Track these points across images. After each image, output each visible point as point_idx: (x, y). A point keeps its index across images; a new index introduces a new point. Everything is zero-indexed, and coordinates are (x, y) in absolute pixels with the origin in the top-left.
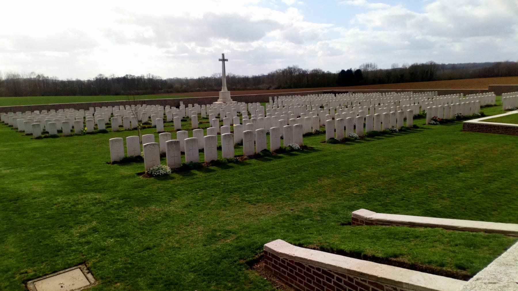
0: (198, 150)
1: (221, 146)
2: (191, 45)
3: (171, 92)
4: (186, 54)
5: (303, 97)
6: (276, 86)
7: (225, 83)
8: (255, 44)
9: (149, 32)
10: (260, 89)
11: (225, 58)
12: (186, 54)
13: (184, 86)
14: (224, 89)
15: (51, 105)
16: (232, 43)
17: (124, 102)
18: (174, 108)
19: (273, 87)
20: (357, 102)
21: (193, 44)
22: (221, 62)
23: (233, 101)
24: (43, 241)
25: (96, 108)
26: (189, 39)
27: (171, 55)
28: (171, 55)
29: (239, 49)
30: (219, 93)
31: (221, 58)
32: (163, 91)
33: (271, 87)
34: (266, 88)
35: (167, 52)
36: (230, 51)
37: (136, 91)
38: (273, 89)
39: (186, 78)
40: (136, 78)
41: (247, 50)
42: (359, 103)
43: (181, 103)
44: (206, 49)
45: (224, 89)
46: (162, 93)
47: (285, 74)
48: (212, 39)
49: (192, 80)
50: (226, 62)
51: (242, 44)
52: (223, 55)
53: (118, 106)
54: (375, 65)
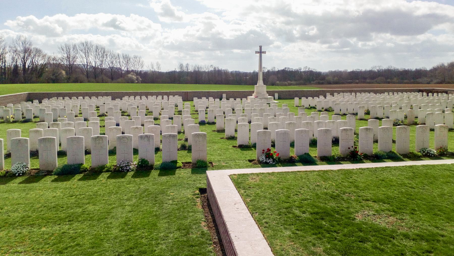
0: (12, 156)
2: (353, 41)
3: (323, 83)
5: (378, 95)
6: (438, 80)
7: (261, 77)
8: (422, 37)
9: (313, 31)
11: (263, 50)
12: (348, 49)
13: (336, 78)
14: (260, 82)
15: (104, 93)
16: (394, 37)
17: (168, 92)
18: (218, 100)
19: (435, 81)
20: (417, 106)
21: (355, 39)
22: (258, 55)
23: (269, 95)
24: (288, 214)
26: (351, 34)
27: (334, 50)
28: (334, 50)
29: (403, 43)
30: (254, 87)
32: (314, 82)
33: (432, 81)
34: (426, 82)
35: (329, 47)
36: (394, 45)
37: (289, 82)
38: (435, 84)
39: (346, 70)
40: (293, 70)
42: (398, 108)
43: (224, 95)
44: (368, 43)
45: (260, 82)
46: (313, 84)
47: (27, 67)
48: (373, 35)
49: (345, 72)
50: (263, 55)
51: (405, 37)
52: (261, 47)
53: (422, 93)
54: (124, 55)
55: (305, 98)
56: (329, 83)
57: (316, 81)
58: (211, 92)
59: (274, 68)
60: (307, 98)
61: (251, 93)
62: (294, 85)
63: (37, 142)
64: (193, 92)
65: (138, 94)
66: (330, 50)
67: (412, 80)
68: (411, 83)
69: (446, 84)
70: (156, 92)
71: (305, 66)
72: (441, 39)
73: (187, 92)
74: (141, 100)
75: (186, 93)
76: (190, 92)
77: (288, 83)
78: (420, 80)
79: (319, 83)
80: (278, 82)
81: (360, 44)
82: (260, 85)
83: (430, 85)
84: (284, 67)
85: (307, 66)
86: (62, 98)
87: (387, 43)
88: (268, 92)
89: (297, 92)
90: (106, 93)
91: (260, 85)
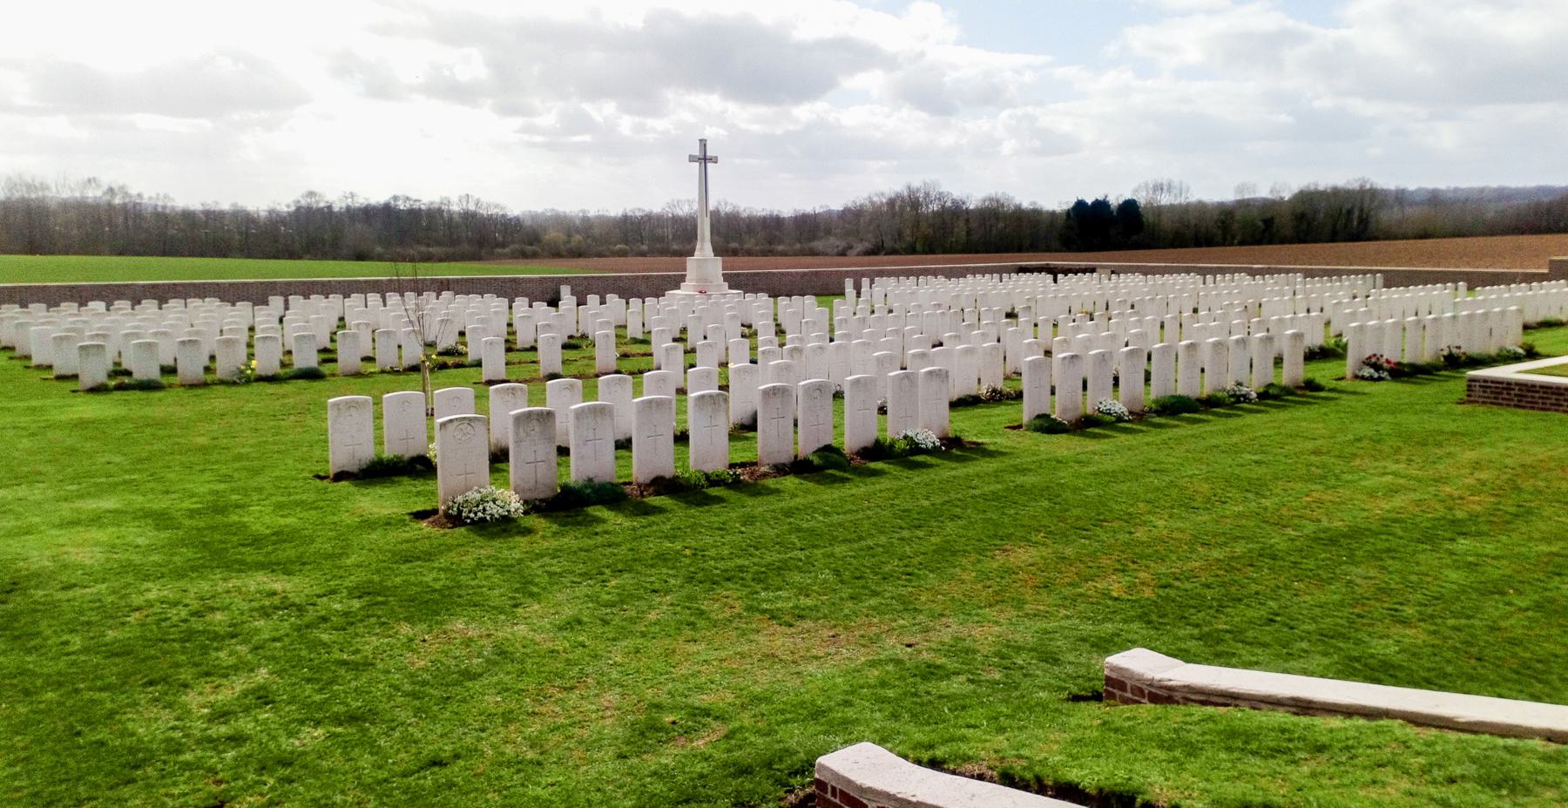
1: (687, 431)
2: (604, 111)
3: (534, 255)
4: (587, 138)
7: (705, 230)
8: (804, 112)
9: (471, 66)
10: (817, 255)
12: (587, 138)
14: (704, 249)
15: (143, 286)
16: (732, 107)
17: (382, 281)
18: (541, 306)
19: (860, 247)
21: (609, 108)
23: (730, 288)
25: (290, 297)
26: (597, 90)
27: (538, 139)
29: (755, 128)
31: (697, 152)
36: (725, 133)
37: (423, 249)
38: (858, 255)
40: (423, 207)
41: (779, 131)
43: (565, 291)
44: (651, 122)
45: (704, 249)
48: (670, 94)
50: (710, 165)
52: (703, 143)
53: (363, 296)
55: (17, 306)
56: (557, 254)
57: (512, 247)
58: (523, 279)
59: (352, 195)
60: (664, 295)
61: (676, 282)
62: (441, 260)
63: (571, 417)
64: (467, 280)
65: (275, 289)
66: (526, 137)
67: (798, 246)
68: (796, 254)
69: (886, 254)
70: (339, 282)
71: (463, 194)
72: (852, 118)
73: (448, 280)
74: (385, 305)
75: (445, 283)
76: (458, 279)
77: (420, 253)
78: (818, 245)
79: (524, 255)
80: (379, 249)
81: (626, 124)
82: (704, 261)
83: (846, 258)
84: (391, 195)
85: (470, 194)
86: (434, 294)
87: (708, 127)
88: (726, 277)
89: (757, 278)
90: (154, 286)
91: (704, 261)
